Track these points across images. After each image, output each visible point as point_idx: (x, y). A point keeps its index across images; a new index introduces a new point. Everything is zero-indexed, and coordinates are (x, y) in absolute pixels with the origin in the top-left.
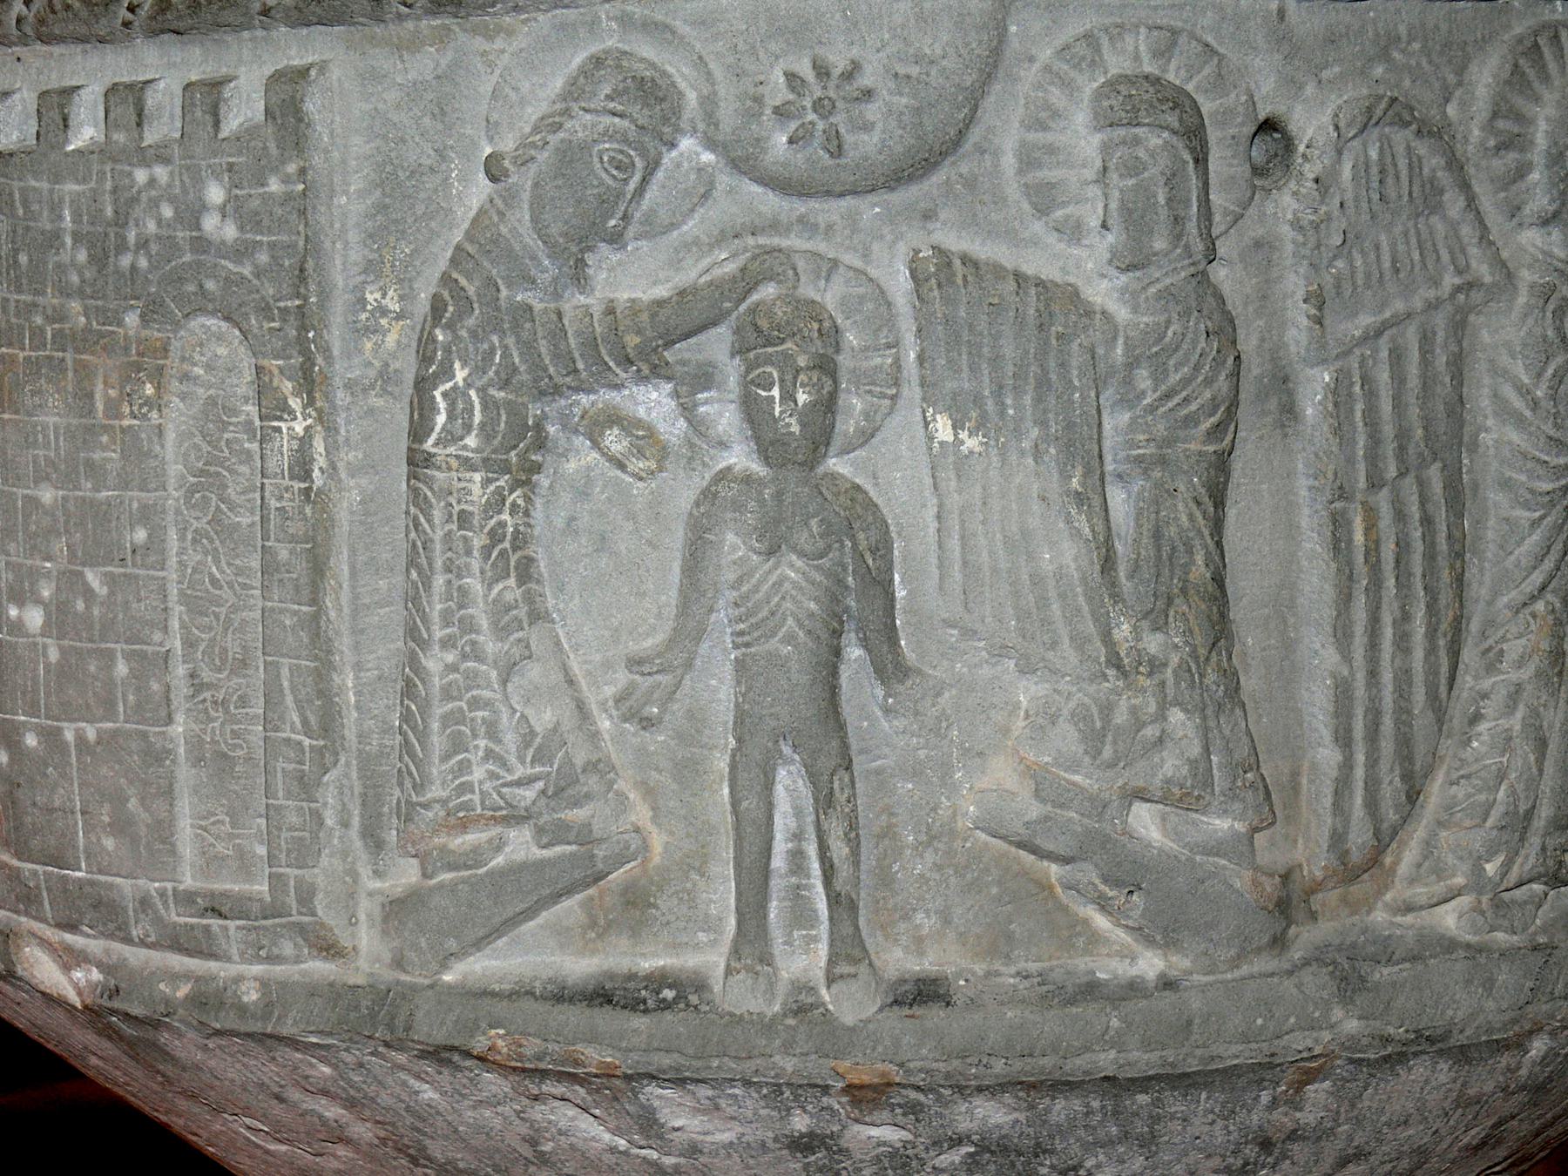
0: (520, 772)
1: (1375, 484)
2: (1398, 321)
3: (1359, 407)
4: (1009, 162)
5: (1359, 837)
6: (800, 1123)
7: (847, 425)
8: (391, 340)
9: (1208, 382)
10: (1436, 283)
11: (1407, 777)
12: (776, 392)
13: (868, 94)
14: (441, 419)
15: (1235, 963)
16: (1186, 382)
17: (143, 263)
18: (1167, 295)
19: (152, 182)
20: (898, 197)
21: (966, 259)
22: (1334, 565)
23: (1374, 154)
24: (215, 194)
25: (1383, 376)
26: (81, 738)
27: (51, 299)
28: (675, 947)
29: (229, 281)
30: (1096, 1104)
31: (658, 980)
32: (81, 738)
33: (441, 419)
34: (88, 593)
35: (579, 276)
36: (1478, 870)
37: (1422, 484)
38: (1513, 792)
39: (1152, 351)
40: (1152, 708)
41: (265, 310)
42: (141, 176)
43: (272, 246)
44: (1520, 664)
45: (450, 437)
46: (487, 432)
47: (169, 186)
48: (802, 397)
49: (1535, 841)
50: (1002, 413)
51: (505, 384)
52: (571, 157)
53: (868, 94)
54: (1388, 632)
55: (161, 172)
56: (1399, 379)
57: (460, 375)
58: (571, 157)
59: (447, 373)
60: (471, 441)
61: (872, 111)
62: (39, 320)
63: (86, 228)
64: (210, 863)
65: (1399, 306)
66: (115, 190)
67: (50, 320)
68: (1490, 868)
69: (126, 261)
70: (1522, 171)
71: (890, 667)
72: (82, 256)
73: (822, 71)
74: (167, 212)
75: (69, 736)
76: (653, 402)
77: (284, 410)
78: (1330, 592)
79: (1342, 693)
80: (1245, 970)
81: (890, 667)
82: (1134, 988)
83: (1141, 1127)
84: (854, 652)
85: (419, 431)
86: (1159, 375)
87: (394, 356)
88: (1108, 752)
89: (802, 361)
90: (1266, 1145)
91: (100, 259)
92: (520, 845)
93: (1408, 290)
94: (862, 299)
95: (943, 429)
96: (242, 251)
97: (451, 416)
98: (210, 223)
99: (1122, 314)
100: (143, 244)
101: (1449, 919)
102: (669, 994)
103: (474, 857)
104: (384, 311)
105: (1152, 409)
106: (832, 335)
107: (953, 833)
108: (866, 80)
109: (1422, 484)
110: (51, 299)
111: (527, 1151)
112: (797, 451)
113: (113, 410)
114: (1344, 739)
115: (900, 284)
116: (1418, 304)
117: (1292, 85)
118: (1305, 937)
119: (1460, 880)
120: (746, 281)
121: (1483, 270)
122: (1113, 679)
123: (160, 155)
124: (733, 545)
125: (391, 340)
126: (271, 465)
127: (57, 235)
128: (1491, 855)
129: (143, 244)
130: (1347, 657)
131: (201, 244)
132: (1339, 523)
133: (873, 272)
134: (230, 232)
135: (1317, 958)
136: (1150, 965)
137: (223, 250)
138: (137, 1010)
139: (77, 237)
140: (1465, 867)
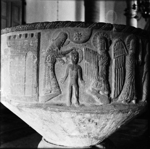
1: (118, 68)
2: (120, 56)
3: (117, 62)
4: (92, 42)
5: (116, 96)
6: (73, 115)
7: (79, 61)
8: (44, 53)
9: (106, 59)
10: (123, 53)
11: (120, 91)
12: (73, 58)
13: (82, 36)
14: (47, 59)
15: (107, 104)
16: (104, 59)
17: (25, 47)
18: (103, 52)
19: (26, 41)
20: (83, 44)
21: (88, 49)
22: (68, 112)
23: (119, 43)
24: (31, 42)
25: (119, 60)
27: (17, 50)
30: (95, 115)
33: (47, 59)
35: (59, 49)
36: (125, 98)
37: (122, 69)
38: (128, 92)
39: (102, 56)
41: (34, 51)
42: (25, 41)
43: (35, 46)
45: (48, 61)
46: (51, 60)
48: (75, 58)
49: (129, 96)
50: (90, 60)
51: (53, 57)
53: (82, 36)
54: (119, 80)
55: (27, 40)
56: (120, 60)
57: (49, 56)
59: (48, 56)
60: (50, 61)
61: (82, 37)
62: (16, 52)
63: (21, 45)
65: (120, 55)
66: (23, 42)
67: (17, 52)
68: (126, 98)
69: (24, 47)
70: (129, 46)
71: (82, 79)
72: (20, 47)
73: (78, 34)
74: (27, 43)
76: (64, 58)
78: (114, 76)
80: (107, 105)
81: (82, 79)
82: (99, 106)
83: (98, 117)
84: (79, 79)
85: (46, 60)
86: (103, 58)
87: (44, 55)
88: (98, 87)
89: (76, 56)
90: (108, 120)
93: (121, 54)
94: (80, 52)
95: (86, 62)
96: (33, 46)
97: (48, 59)
99: (100, 53)
101: (123, 102)
102: (63, 105)
104: (43, 51)
105: (102, 61)
106: (78, 54)
107: (85, 93)
108: (81, 35)
109: (122, 69)
110: (17, 50)
111: (51, 118)
112: (76, 62)
114: (115, 87)
115: (84, 50)
116: (122, 55)
117: (113, 38)
118: (112, 103)
119: (123, 99)
120: (72, 50)
121: (126, 53)
122: (98, 81)
125: (44, 53)
126: (34, 63)
128: (126, 97)
129: (25, 46)
130: (116, 81)
131: (30, 46)
132: (115, 71)
133: (81, 49)
135: (113, 104)
136: (101, 104)
138: (21, 106)
139: (20, 46)
140: (124, 98)
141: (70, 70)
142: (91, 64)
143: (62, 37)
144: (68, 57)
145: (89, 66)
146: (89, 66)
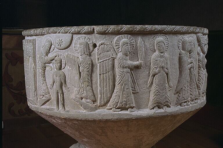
0: (43, 92)
40: (83, 90)
44: (118, 89)
79: (100, 91)
142: (73, 71)
143: (48, 45)
145: (72, 72)
146: (72, 72)
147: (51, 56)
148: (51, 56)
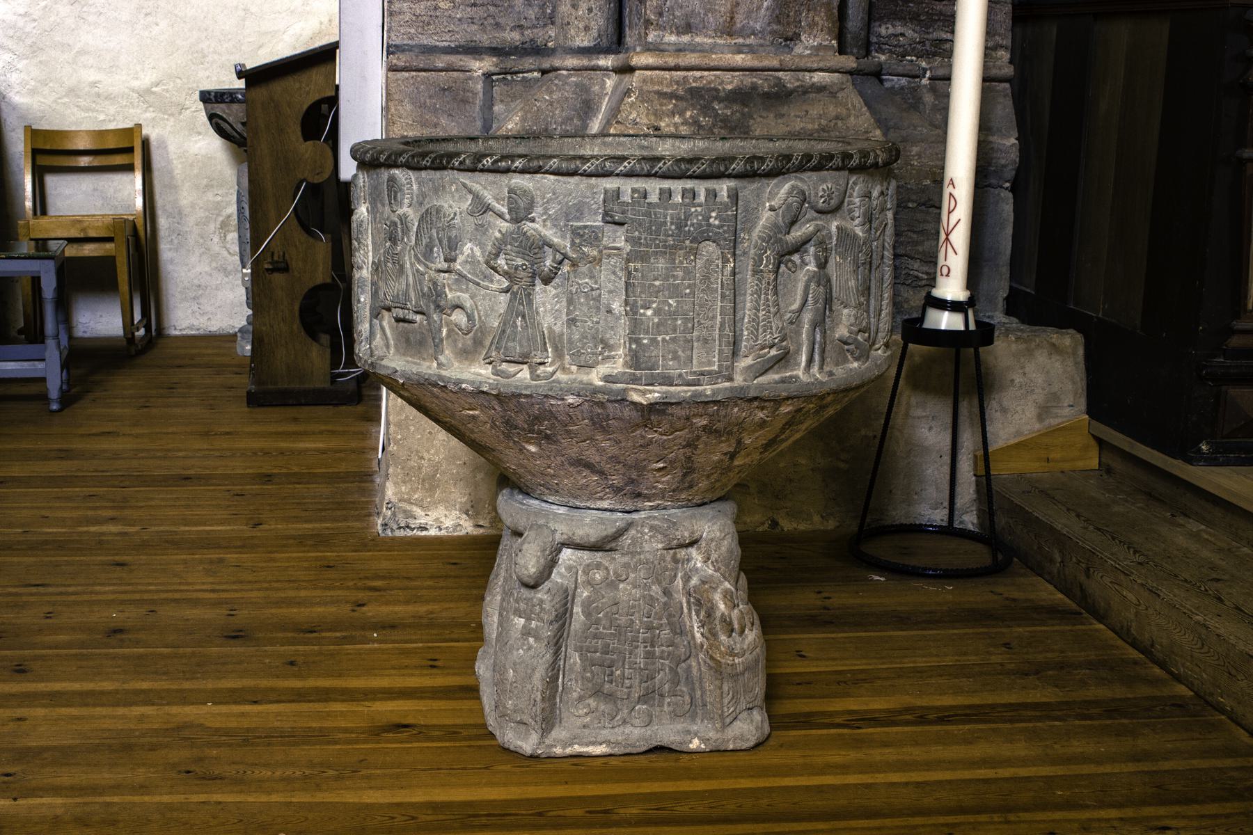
26: (664, 340)
28: (396, 345)
29: (716, 233)
31: (791, 377)
32: (664, 340)
34: (670, 305)
41: (725, 239)
45: (766, 266)
47: (1235, 332)
52: (789, 206)
55: (699, 209)
58: (789, 206)
64: (701, 364)
75: (660, 338)
77: (728, 261)
91: (679, 228)
92: (773, 352)
96: (719, 227)
98: (712, 220)
100: (692, 225)
103: (765, 355)
113: (681, 262)
123: (700, 205)
124: (813, 286)
127: (665, 223)
129: (692, 225)
131: (709, 225)
134: (717, 222)
137: (714, 226)
141: (813, 286)
144: (806, 251)
147: (797, 233)
148: (797, 233)
